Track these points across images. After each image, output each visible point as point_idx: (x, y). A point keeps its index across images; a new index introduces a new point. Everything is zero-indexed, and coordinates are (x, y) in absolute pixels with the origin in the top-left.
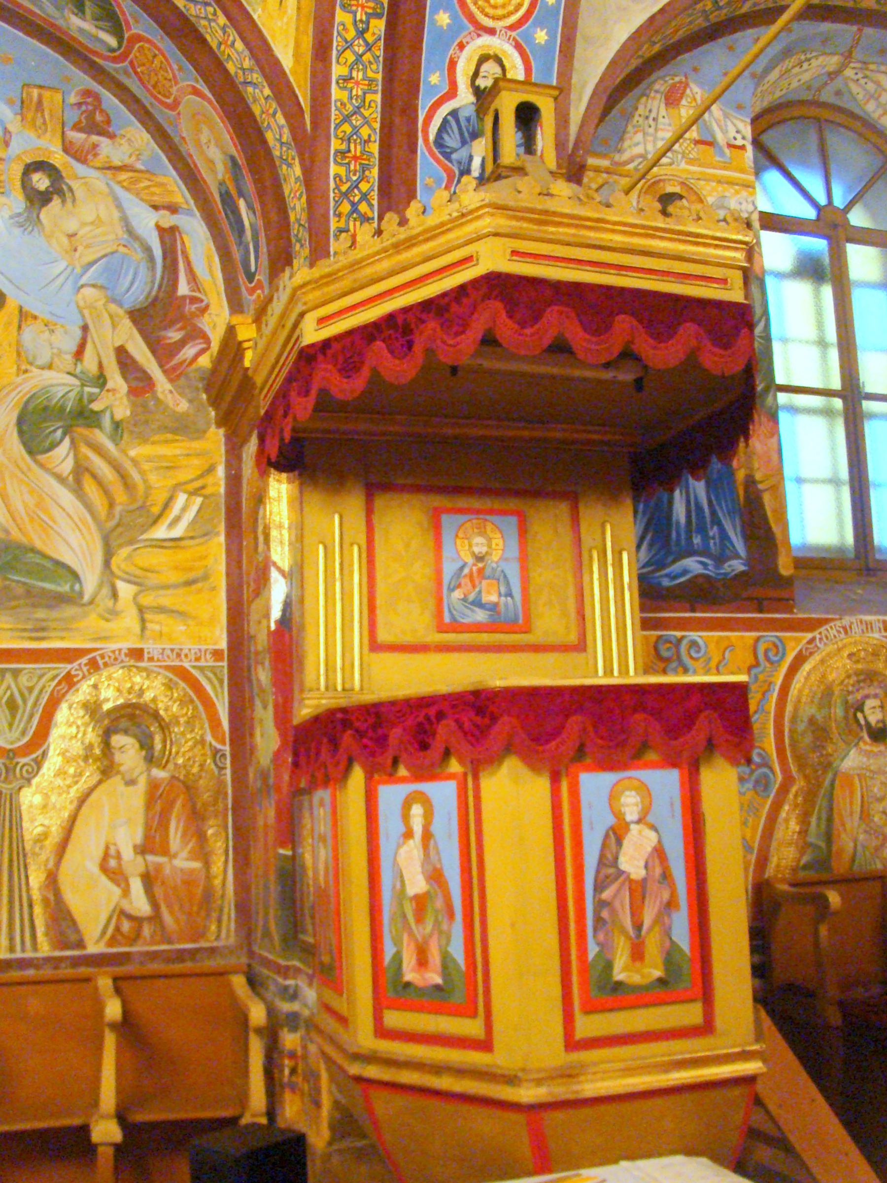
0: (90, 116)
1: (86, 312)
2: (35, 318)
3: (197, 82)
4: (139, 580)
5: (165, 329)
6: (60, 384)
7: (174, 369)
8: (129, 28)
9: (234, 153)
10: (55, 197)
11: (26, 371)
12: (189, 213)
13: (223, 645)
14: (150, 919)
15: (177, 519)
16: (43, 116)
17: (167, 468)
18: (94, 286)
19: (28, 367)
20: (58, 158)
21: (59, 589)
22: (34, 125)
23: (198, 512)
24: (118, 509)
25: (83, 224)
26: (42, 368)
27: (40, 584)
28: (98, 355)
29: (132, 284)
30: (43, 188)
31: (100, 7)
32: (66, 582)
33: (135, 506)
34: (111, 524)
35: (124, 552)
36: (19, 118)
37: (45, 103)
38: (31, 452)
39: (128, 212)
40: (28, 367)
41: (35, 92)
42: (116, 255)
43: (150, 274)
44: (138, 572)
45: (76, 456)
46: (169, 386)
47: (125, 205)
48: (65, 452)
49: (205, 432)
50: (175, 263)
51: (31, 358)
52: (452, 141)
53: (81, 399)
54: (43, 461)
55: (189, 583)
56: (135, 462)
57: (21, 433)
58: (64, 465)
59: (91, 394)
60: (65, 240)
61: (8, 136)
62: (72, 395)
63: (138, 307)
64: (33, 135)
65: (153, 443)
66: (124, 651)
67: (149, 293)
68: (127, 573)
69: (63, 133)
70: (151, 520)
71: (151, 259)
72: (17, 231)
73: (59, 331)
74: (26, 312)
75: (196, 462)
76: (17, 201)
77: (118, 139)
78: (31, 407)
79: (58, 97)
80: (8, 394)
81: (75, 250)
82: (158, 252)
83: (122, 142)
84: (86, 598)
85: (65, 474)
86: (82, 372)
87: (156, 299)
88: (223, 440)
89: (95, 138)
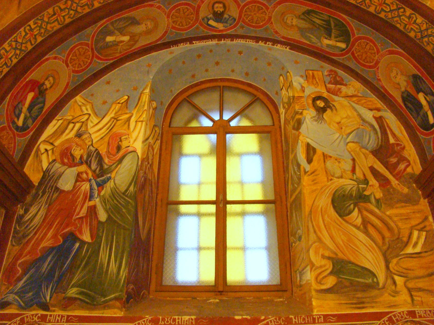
0: (335, 78)
1: (352, 153)
2: (331, 157)
3: (392, 46)
4: (405, 275)
5: (389, 157)
6: (348, 184)
7: (398, 174)
8: (354, 35)
9: (416, 72)
10: (328, 109)
11: (331, 180)
12: (385, 110)
16: (316, 80)
17: (406, 219)
18: (353, 142)
19: (332, 178)
20: (325, 94)
21: (367, 281)
22: (313, 84)
23: (426, 239)
24: (387, 240)
25: (342, 118)
26: (338, 178)
27: (357, 279)
28: (362, 170)
29: (369, 140)
31: (339, 30)
32: (369, 278)
33: (395, 238)
34: (385, 248)
35: (395, 261)
36: (306, 82)
37: (316, 76)
38: (340, 216)
39: (360, 112)
40: (332, 178)
41: (311, 72)
42: (359, 129)
43: (376, 135)
44: (404, 271)
45: (362, 215)
46: (397, 182)
47: (358, 109)
48: (356, 215)
49: (419, 201)
50: (385, 130)
51: (332, 174)
53: (359, 190)
54: (347, 220)
56: (389, 216)
57: (334, 207)
58: (357, 221)
59: (363, 188)
60: (336, 125)
61: (303, 89)
62: (354, 189)
63: (374, 149)
64: (313, 87)
65: (397, 208)
66: (405, 312)
67: (378, 143)
68: (397, 271)
69: (325, 85)
70: (404, 244)
72: (315, 123)
73: (343, 163)
74: (326, 155)
75: (418, 215)
77: (348, 86)
78: (337, 194)
79: (320, 73)
80: (325, 190)
81: (342, 128)
82: (377, 127)
83: (350, 87)
84: (381, 285)
85: (359, 225)
86: (357, 178)
87: (381, 146)
88: (428, 204)
89: (339, 86)
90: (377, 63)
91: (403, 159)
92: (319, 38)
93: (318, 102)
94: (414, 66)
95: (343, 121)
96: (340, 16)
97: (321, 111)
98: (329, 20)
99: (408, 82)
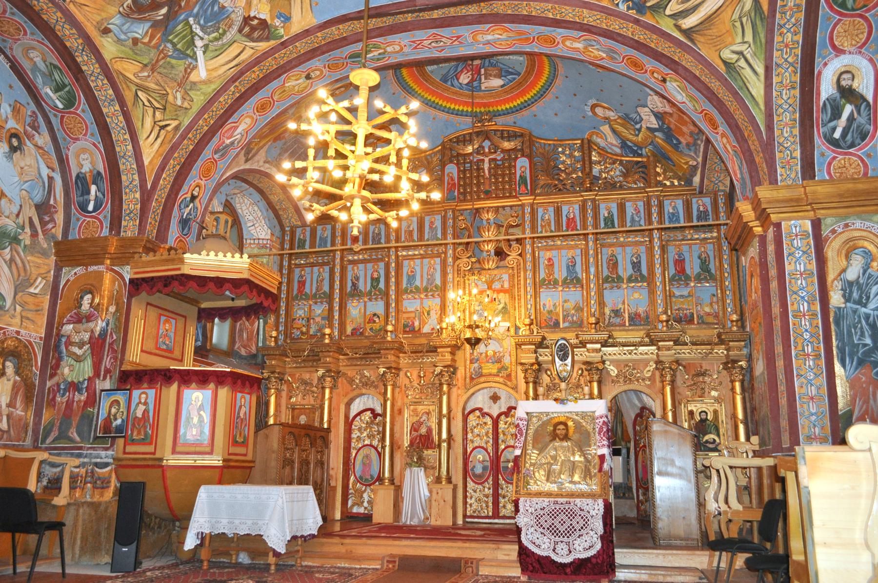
0: (34, 121)
13: (43, 336)
14: (6, 432)
15: (37, 286)
30: (16, 144)
35: (20, 294)
52: (182, 206)
55: (37, 311)
71: (44, 187)
72: (5, 159)
76: (6, 148)
90: (78, 139)
91: (52, 220)
92: (44, 84)
93: (14, 140)
94: (105, 168)
95: (26, 168)
96: (77, 91)
97: (13, 149)
98: (66, 86)
99: (91, 171)
